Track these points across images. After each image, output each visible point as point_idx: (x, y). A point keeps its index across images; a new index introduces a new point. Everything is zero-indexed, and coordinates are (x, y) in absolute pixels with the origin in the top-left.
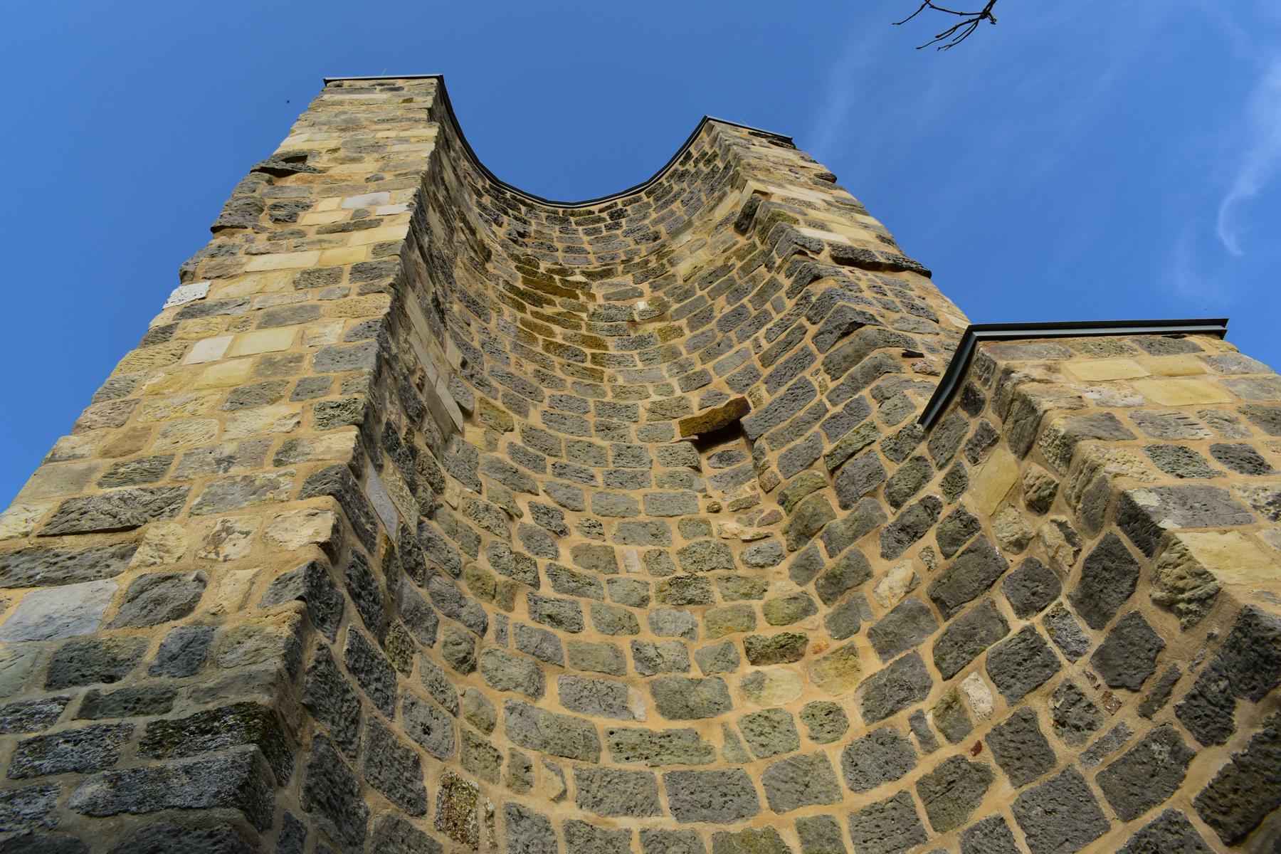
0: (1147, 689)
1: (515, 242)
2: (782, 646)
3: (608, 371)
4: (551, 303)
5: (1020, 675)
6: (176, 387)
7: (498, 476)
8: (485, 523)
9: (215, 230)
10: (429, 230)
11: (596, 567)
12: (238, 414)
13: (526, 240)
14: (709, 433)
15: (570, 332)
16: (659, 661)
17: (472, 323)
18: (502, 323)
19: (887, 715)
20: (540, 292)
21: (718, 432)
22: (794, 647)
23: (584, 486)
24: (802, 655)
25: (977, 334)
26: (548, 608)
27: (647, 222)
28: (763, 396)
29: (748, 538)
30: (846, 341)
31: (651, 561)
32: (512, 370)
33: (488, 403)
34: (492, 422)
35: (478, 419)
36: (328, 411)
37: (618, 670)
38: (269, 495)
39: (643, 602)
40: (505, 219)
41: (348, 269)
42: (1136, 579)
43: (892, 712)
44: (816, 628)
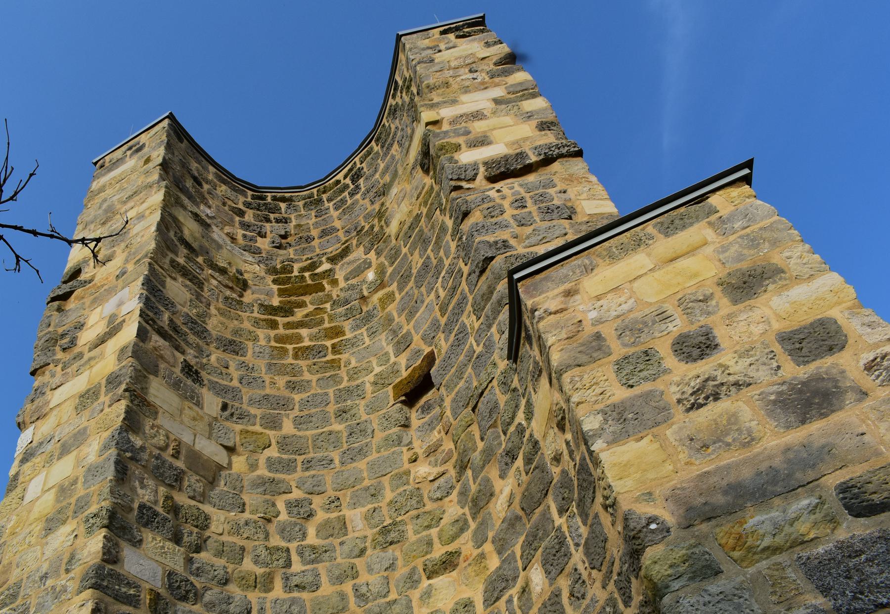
0: (604, 569)
1: (279, 247)
2: (444, 563)
3: (344, 357)
4: (302, 305)
5: (555, 563)
6: (22, 525)
7: (259, 490)
8: (245, 536)
9: (33, 373)
10: (169, 304)
11: (332, 535)
12: (49, 538)
13: (289, 239)
14: (411, 391)
15: (315, 330)
16: (369, 594)
17: (231, 363)
18: (257, 350)
19: (495, 602)
20: (293, 298)
21: (417, 389)
22: (451, 561)
23: (326, 471)
24: (457, 565)
25: (516, 276)
26: (296, 580)
27: (377, 176)
28: (443, 344)
29: (432, 478)
30: (483, 278)
31: (368, 517)
32: (268, 391)
33: (247, 432)
34: (251, 448)
35: (240, 449)
36: (91, 521)
37: (343, 608)
38: (63, 597)
39: (362, 552)
40: (268, 226)
41: (104, 382)
42: (594, 487)
43: (498, 599)
44: (465, 544)
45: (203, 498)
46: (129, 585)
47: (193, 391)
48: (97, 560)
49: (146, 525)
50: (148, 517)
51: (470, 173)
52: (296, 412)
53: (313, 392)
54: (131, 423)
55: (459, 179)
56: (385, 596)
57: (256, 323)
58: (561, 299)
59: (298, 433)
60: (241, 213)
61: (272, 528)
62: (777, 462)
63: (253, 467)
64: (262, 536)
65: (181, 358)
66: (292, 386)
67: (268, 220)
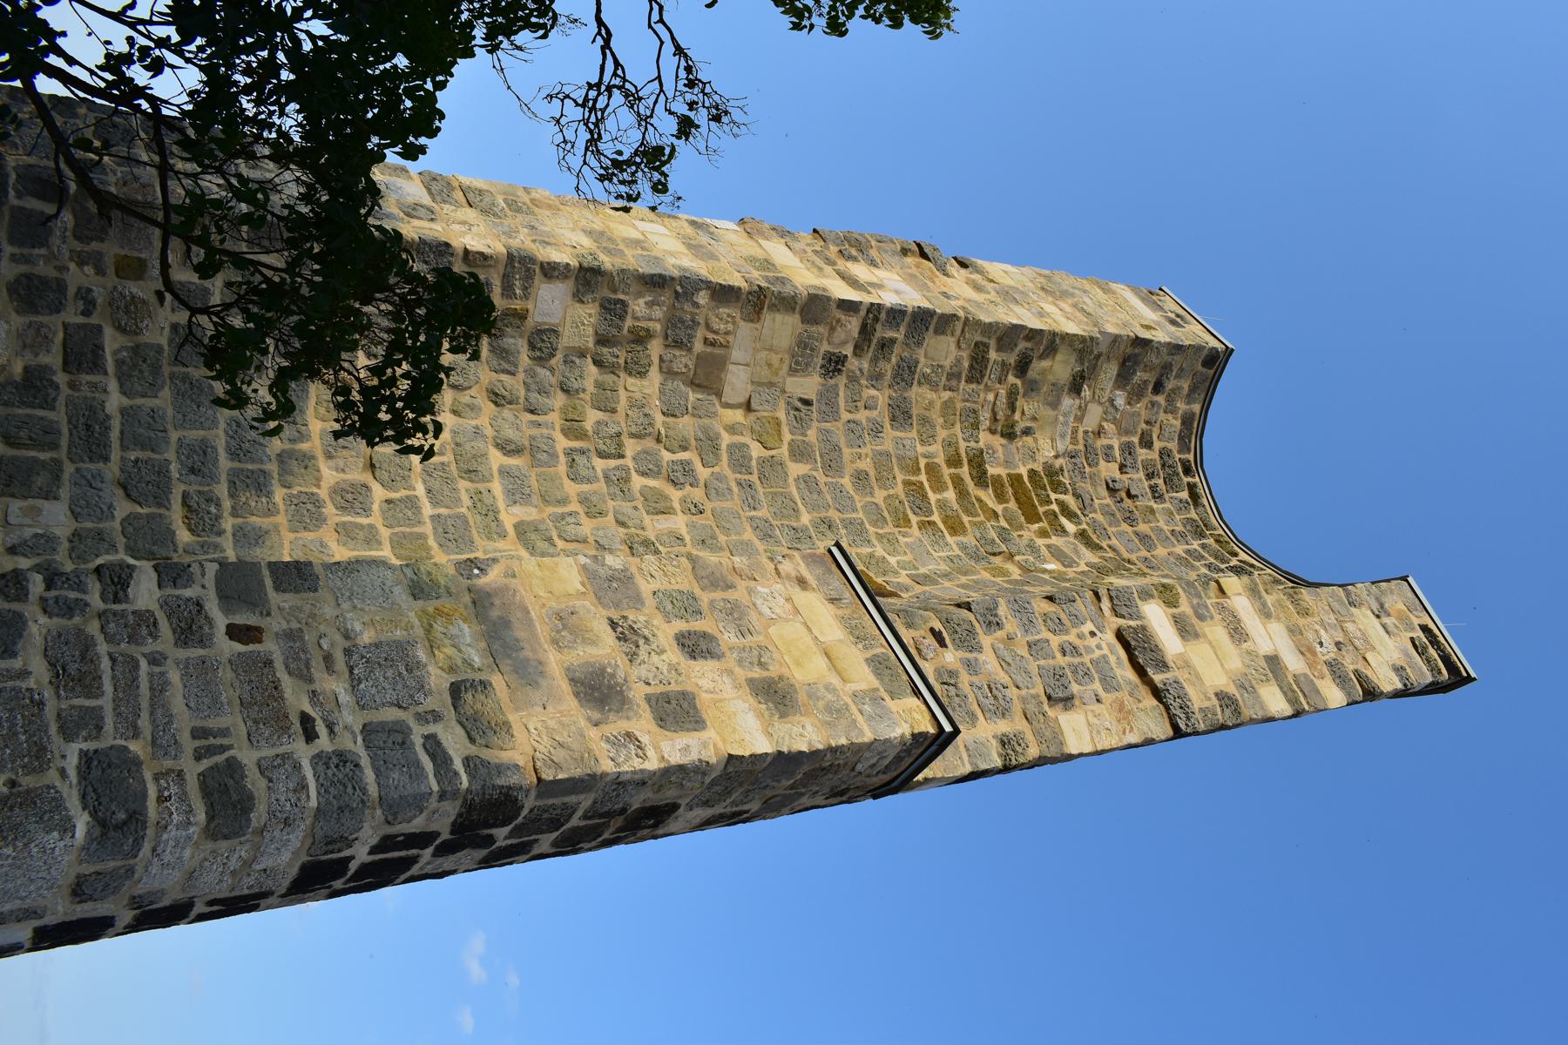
9: (815, 231)
32: (846, 452)
45: (668, 372)
46: (525, 289)
47: (808, 365)
48: (540, 258)
49: (602, 306)
50: (614, 310)
51: (1124, 611)
52: (822, 479)
53: (857, 498)
54: (724, 294)
55: (1111, 598)
56: (560, 536)
57: (949, 444)
58: (793, 574)
59: (791, 480)
60: (1147, 443)
61: (650, 443)
62: (527, 653)
63: (732, 429)
64: (634, 430)
65: (848, 350)
66: (860, 478)
67: (1150, 476)
